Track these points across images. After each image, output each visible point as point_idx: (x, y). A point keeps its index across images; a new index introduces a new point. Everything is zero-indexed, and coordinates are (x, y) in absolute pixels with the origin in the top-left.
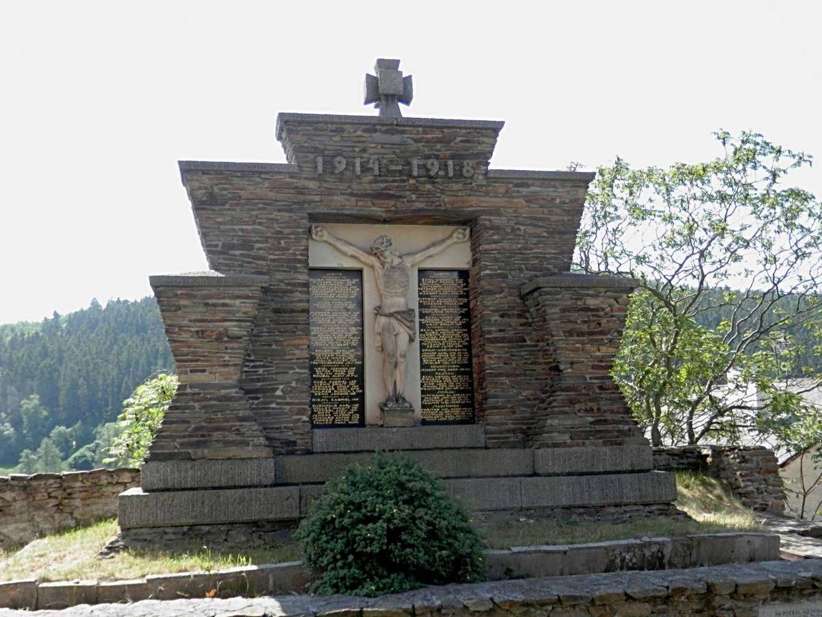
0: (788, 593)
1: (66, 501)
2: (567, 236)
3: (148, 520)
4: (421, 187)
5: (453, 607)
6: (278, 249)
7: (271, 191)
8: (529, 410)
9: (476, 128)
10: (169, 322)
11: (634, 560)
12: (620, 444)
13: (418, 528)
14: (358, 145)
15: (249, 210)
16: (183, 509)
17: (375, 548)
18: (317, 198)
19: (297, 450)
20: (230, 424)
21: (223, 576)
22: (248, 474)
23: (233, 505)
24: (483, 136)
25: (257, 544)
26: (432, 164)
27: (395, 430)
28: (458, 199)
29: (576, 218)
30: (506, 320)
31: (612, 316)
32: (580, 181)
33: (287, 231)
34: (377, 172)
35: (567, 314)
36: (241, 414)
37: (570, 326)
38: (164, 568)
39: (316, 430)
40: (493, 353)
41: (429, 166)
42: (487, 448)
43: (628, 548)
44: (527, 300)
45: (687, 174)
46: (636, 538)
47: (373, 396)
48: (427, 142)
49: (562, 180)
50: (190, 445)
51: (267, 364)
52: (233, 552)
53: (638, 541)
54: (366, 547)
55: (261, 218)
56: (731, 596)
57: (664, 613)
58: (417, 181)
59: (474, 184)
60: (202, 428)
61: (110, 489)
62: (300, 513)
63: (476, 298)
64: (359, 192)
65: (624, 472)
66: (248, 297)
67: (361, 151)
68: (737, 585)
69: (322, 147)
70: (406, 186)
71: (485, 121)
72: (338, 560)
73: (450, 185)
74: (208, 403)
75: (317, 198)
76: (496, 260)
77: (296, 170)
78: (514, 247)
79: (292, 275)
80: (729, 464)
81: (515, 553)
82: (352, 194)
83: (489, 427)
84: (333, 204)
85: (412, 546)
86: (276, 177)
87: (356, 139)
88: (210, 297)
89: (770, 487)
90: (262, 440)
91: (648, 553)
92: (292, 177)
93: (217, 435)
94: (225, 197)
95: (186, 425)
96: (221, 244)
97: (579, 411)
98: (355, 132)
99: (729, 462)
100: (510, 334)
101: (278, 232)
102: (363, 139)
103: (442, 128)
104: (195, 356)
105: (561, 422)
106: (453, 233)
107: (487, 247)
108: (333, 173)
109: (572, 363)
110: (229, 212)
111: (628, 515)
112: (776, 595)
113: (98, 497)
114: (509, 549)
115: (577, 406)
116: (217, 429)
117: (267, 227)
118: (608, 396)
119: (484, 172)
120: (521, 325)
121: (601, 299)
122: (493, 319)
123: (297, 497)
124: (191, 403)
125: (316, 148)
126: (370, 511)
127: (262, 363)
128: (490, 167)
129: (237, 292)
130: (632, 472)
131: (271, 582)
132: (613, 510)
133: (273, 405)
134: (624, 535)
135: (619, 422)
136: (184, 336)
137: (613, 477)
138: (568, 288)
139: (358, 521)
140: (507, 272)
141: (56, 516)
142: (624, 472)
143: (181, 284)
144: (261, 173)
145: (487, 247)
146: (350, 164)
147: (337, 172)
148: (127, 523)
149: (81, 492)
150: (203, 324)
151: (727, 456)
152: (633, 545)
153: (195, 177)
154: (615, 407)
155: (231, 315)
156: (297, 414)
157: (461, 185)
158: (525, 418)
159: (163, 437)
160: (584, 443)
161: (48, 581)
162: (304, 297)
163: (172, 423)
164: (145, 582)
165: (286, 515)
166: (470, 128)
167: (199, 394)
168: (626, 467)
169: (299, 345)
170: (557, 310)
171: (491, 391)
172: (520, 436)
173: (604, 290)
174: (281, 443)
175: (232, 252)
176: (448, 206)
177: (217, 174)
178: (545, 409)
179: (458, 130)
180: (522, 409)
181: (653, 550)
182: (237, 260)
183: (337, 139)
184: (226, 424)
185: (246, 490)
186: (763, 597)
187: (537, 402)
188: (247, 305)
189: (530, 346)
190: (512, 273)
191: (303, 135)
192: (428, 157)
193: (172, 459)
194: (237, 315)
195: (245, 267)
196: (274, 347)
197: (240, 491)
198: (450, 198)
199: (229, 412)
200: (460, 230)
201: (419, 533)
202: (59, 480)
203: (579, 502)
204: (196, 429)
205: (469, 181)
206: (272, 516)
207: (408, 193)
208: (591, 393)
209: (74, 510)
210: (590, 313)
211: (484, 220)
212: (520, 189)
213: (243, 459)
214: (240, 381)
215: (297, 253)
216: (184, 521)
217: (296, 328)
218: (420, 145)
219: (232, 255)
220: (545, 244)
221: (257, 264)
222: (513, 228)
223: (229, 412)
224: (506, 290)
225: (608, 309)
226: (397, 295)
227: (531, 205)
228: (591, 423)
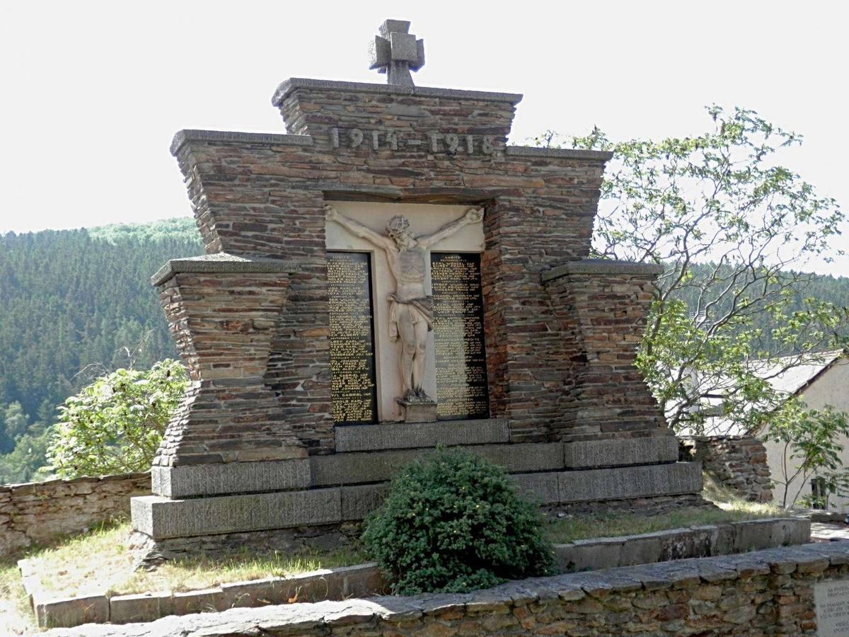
0: (838, 571)
1: (19, 517)
2: (585, 219)
3: (185, 530)
4: (439, 164)
5: (550, 598)
6: (294, 230)
7: (283, 165)
8: (551, 402)
9: (494, 101)
10: (192, 312)
11: (684, 549)
12: (648, 435)
13: (498, 523)
14: (375, 116)
15: (261, 186)
16: (221, 516)
17: (459, 545)
18: (333, 174)
19: (321, 450)
20: (260, 423)
21: (300, 581)
22: (284, 477)
23: (272, 510)
24: (500, 109)
25: (304, 550)
26: (452, 139)
27: (418, 426)
28: (478, 177)
29: (594, 200)
30: (528, 307)
31: (638, 304)
32: (597, 160)
33: (302, 210)
34: (395, 147)
35: (594, 301)
36: (270, 411)
37: (598, 314)
38: (201, 581)
39: (338, 428)
40: (515, 343)
41: (448, 141)
42: (510, 443)
43: (680, 537)
44: (548, 286)
45: (677, 149)
46: (685, 527)
47: (388, 390)
48: (444, 115)
49: (580, 159)
50: (222, 446)
51: (286, 357)
52: (287, 557)
53: (688, 530)
54: (450, 544)
55: (274, 196)
56: (792, 576)
57: (732, 594)
58: (435, 157)
59: (492, 162)
60: (230, 428)
61: (68, 501)
62: (343, 516)
63: (492, 283)
64: (376, 168)
65: (652, 464)
66: (275, 284)
67: (376, 123)
68: (797, 565)
69: (336, 117)
70: (423, 162)
71: (503, 94)
72: (422, 559)
73: (469, 162)
74: (234, 401)
75: (333, 174)
76: (517, 244)
77: (310, 142)
78: (534, 230)
79: (309, 259)
80: (716, 454)
81: (578, 546)
82: (369, 171)
83: (513, 421)
84: (350, 181)
85: (494, 541)
86: (289, 150)
87: (371, 110)
88: (236, 284)
89: (759, 477)
90: (295, 440)
91: (697, 541)
92: (305, 150)
93: (247, 436)
94: (235, 172)
95: (212, 426)
96: (231, 224)
97: (607, 403)
98: (370, 101)
99: (716, 453)
100: (532, 322)
101: (294, 212)
102: (379, 110)
103: (460, 99)
104: (218, 349)
105: (592, 414)
106: (467, 212)
107: (507, 229)
108: (348, 146)
109: (598, 353)
110: (239, 189)
111: (660, 507)
112: (828, 573)
113: (55, 512)
114: (571, 543)
115: (605, 398)
116: (247, 429)
117: (280, 206)
118: (634, 387)
119: (503, 149)
120: (543, 313)
121: (627, 286)
122: (515, 306)
123: (338, 500)
124: (217, 401)
125: (330, 119)
126: (449, 508)
127: (280, 356)
128: (508, 144)
129: (265, 278)
130: (660, 463)
131: (345, 585)
132: (645, 502)
133: (294, 402)
134: (674, 524)
135: (644, 413)
136: (207, 328)
137: (645, 468)
138: (596, 275)
139: (437, 520)
140: (527, 256)
141: (8, 535)
142: (652, 464)
143: (206, 270)
144: (273, 145)
145: (507, 229)
146: (368, 137)
147: (354, 146)
148: (162, 533)
149: (34, 506)
150: (228, 314)
151: (714, 446)
152: (684, 534)
153: (201, 149)
154: (641, 398)
155: (257, 304)
156: (320, 411)
157: (479, 162)
158: (548, 411)
159: (191, 439)
160: (613, 435)
161: (116, 594)
162: (322, 283)
163: (199, 423)
164: (221, 591)
165: (328, 519)
166: (488, 101)
167: (224, 391)
168: (654, 458)
169: (319, 336)
170: (585, 298)
171: (514, 382)
172: (544, 430)
173: (630, 276)
174: (304, 443)
175: (243, 233)
176: (467, 185)
177: (225, 145)
178: (572, 401)
179: (476, 102)
180: (545, 401)
181: (701, 538)
182: (250, 242)
183: (351, 108)
184: (255, 423)
185: (286, 494)
186: (818, 575)
187: (559, 394)
188: (275, 293)
189: (549, 335)
190: (533, 257)
191: (316, 103)
192: (447, 131)
193: (202, 463)
194: (263, 304)
195: (259, 250)
196: (292, 338)
197: (280, 494)
198: (473, 176)
199: (258, 410)
200: (474, 211)
201: (500, 528)
202: (8, 494)
203: (613, 496)
204: (225, 429)
205: (488, 158)
206: (313, 521)
207: (426, 170)
208: (617, 383)
209: (27, 527)
210: (617, 301)
211: (503, 200)
212: (538, 168)
213: (277, 461)
214: (266, 376)
215: (314, 234)
216: (223, 529)
217: (315, 317)
218: (438, 117)
219: (244, 236)
220: (564, 227)
221: (271, 247)
222: (532, 209)
223: (258, 410)
224: (527, 276)
225: (633, 297)
226: (414, 280)
227: (550, 185)
228: (619, 415)
